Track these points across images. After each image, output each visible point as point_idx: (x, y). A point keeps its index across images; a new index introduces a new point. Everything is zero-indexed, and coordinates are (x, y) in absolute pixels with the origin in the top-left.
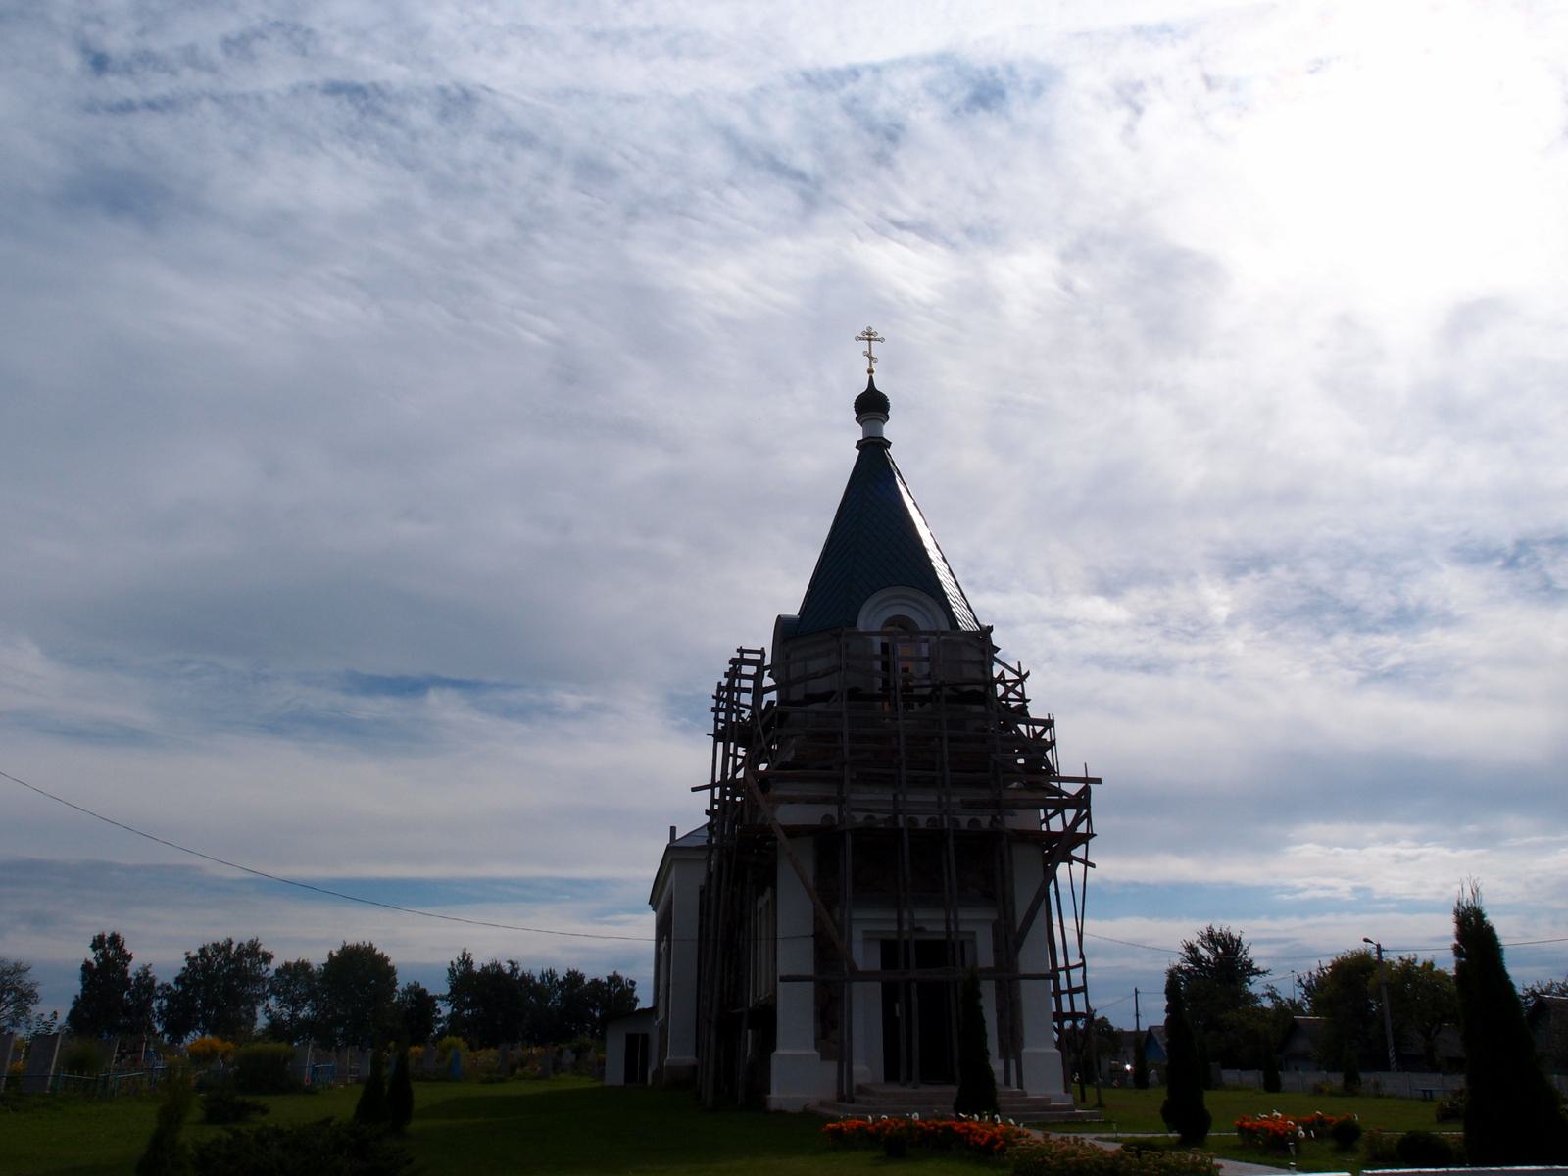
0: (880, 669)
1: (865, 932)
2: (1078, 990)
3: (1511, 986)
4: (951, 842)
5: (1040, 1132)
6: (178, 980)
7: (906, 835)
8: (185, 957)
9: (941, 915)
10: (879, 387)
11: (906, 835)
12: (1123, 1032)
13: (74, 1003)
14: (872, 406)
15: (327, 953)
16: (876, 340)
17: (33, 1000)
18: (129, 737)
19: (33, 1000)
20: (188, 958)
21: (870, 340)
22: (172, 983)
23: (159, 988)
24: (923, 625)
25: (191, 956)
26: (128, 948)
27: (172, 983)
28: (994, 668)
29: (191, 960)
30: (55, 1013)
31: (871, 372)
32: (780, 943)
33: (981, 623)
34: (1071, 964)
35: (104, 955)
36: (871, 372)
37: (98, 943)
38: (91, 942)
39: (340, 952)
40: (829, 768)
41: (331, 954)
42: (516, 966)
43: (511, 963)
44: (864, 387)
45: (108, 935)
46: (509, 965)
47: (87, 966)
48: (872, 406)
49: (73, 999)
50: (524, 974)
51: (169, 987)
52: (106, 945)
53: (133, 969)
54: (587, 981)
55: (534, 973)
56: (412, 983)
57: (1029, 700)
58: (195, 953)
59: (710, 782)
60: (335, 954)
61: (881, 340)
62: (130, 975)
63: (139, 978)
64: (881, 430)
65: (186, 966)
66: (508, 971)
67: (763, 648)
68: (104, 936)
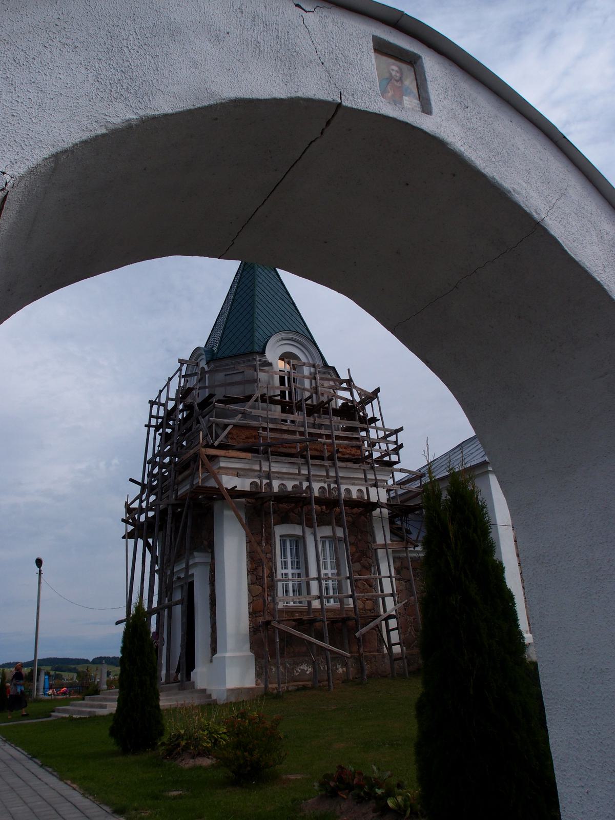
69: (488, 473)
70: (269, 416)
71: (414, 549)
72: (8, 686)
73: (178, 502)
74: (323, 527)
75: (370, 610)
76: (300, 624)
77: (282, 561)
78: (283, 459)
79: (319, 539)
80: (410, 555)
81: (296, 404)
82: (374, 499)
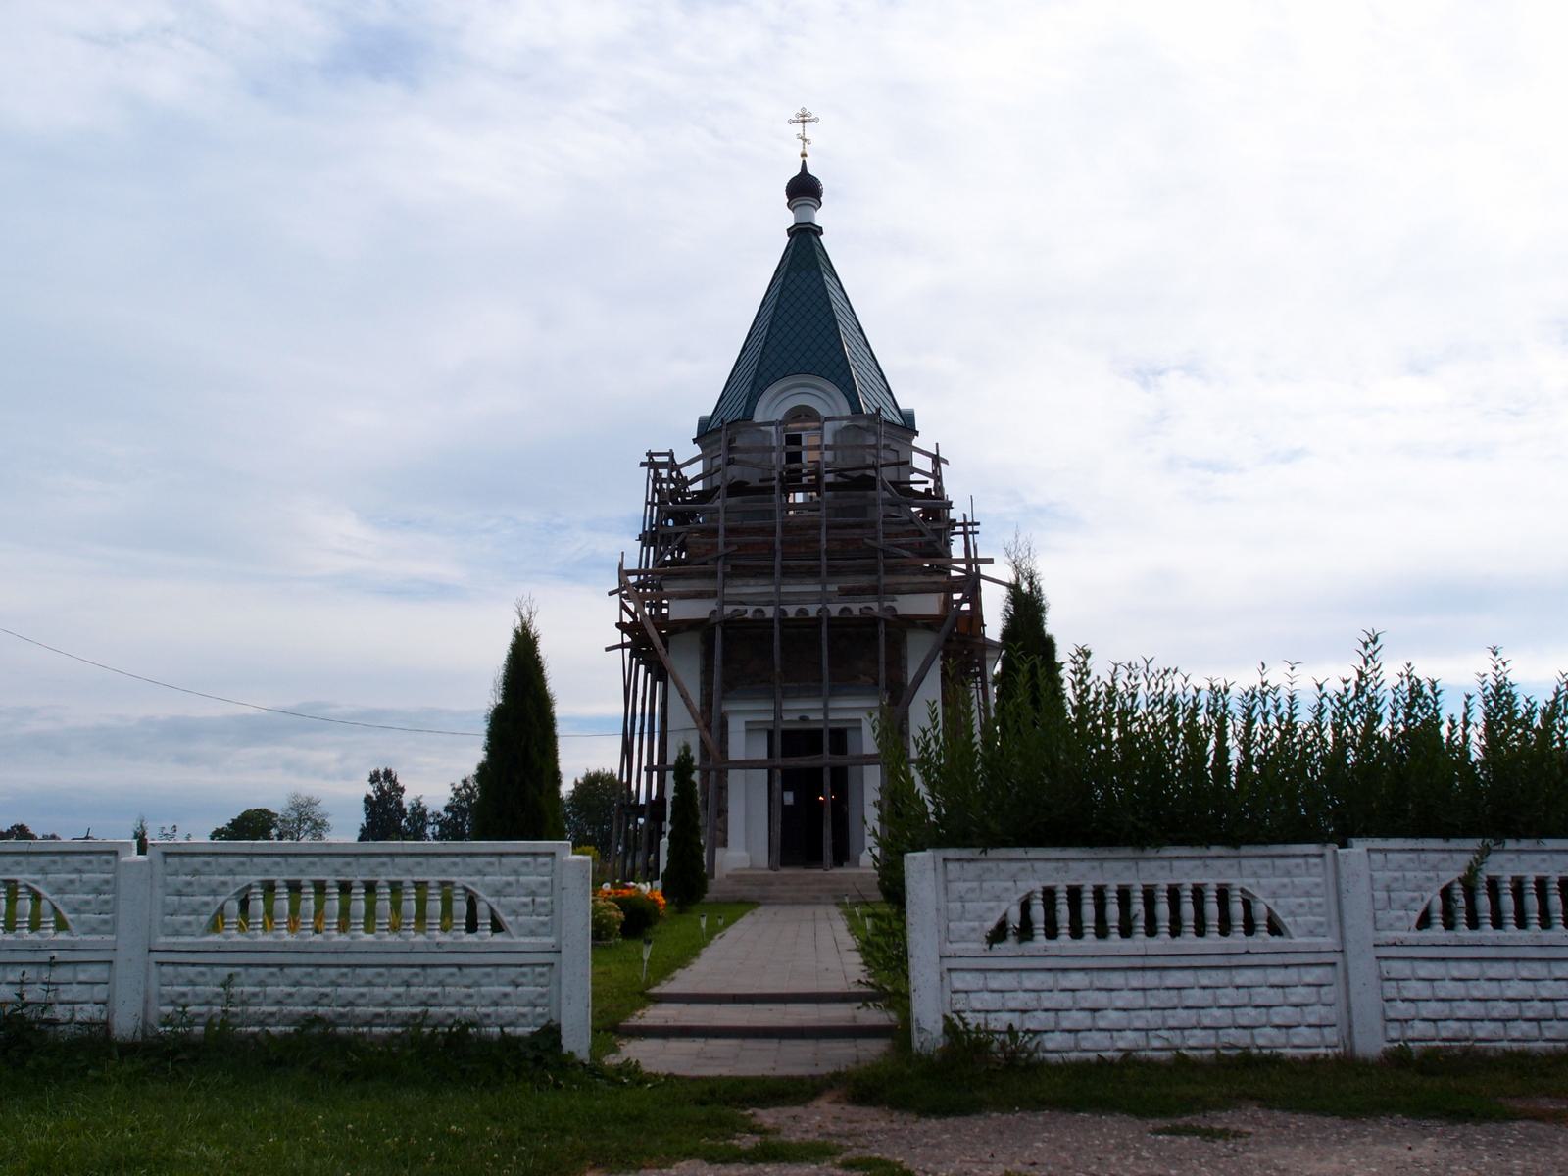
1: (747, 723)
4: (824, 629)
6: (448, 809)
7: (777, 626)
8: (451, 788)
9: (818, 704)
10: (811, 171)
11: (777, 626)
13: (361, 830)
14: (804, 189)
15: (573, 781)
16: (810, 121)
17: (325, 828)
18: (439, 591)
19: (325, 828)
20: (453, 789)
21: (803, 121)
22: (442, 811)
23: (432, 816)
24: (824, 412)
25: (456, 787)
26: (401, 782)
27: (442, 811)
29: (457, 792)
30: (175, 827)
31: (804, 155)
33: (901, 407)
35: (381, 788)
36: (804, 155)
37: (374, 778)
38: (369, 777)
40: (705, 564)
41: (576, 782)
44: (797, 172)
45: (382, 771)
47: (368, 799)
48: (804, 189)
49: (360, 827)
51: (439, 815)
52: (382, 779)
53: (407, 799)
54: (676, 794)
57: (643, 464)
58: (458, 784)
60: (580, 781)
61: (816, 120)
62: (404, 806)
63: (413, 808)
64: (813, 216)
65: (452, 795)
67: (671, 450)
68: (379, 772)
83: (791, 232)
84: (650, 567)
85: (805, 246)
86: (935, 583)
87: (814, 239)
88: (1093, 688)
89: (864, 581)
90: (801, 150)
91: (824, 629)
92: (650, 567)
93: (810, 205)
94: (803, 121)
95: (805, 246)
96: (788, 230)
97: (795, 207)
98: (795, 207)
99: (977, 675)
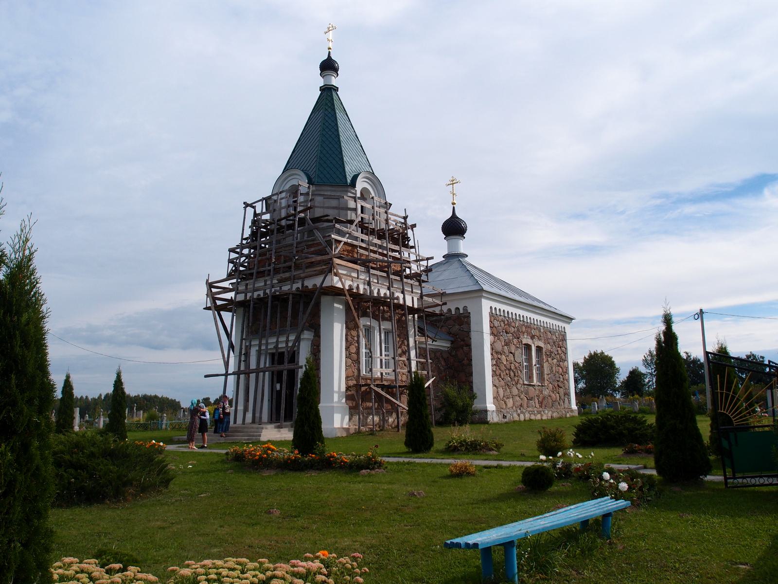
0: (577, 415)
2: (252, 371)
3: (42, 366)
5: (655, 421)
10: (458, 214)
12: (488, 530)
14: (329, 66)
28: (699, 425)
32: (322, 209)
34: (224, 372)
39: (589, 356)
41: (585, 357)
42: (689, 355)
43: (687, 353)
44: (326, 57)
46: (685, 354)
48: (329, 66)
50: (694, 358)
55: (618, 360)
56: (634, 368)
59: (228, 376)
60: (587, 357)
66: (685, 358)
69: (482, 297)
70: (367, 237)
71: (432, 342)
72: (275, 418)
73: (298, 293)
74: (385, 322)
75: (404, 381)
76: (383, 387)
77: (388, 345)
78: (535, 303)
79: (382, 330)
80: (428, 347)
81: (377, 230)
82: (409, 303)
83: (322, 89)
84: (267, 365)
85: (328, 93)
86: (315, 271)
87: (334, 93)
88: (416, 468)
89: (287, 275)
90: (451, 201)
91: (252, 302)
92: (267, 365)
93: (329, 75)
94: (453, 184)
95: (328, 93)
96: (320, 87)
97: (324, 76)
98: (324, 76)
99: (245, 239)
